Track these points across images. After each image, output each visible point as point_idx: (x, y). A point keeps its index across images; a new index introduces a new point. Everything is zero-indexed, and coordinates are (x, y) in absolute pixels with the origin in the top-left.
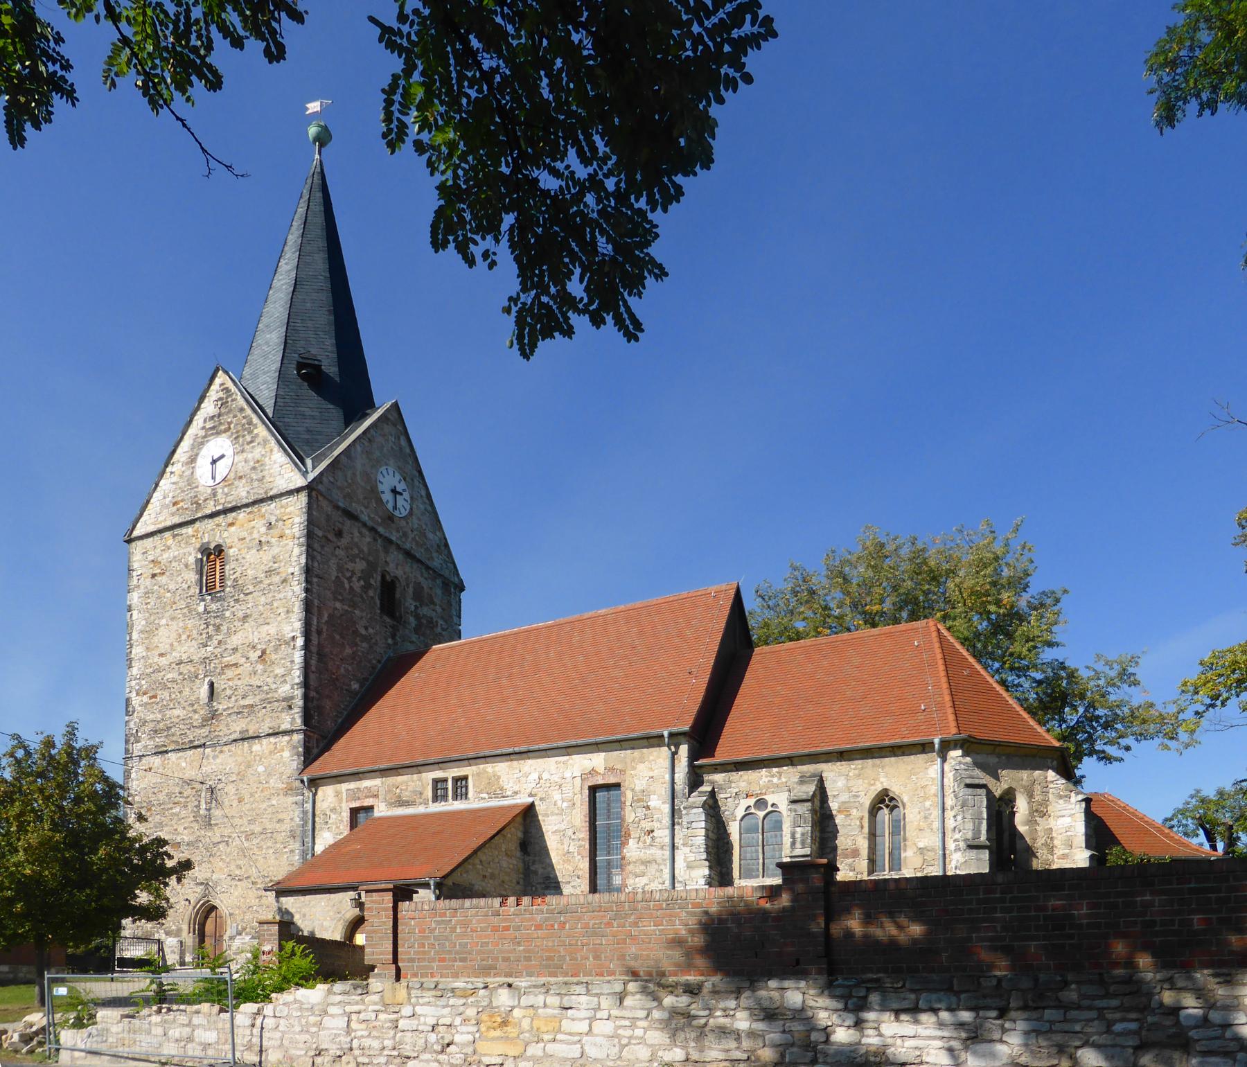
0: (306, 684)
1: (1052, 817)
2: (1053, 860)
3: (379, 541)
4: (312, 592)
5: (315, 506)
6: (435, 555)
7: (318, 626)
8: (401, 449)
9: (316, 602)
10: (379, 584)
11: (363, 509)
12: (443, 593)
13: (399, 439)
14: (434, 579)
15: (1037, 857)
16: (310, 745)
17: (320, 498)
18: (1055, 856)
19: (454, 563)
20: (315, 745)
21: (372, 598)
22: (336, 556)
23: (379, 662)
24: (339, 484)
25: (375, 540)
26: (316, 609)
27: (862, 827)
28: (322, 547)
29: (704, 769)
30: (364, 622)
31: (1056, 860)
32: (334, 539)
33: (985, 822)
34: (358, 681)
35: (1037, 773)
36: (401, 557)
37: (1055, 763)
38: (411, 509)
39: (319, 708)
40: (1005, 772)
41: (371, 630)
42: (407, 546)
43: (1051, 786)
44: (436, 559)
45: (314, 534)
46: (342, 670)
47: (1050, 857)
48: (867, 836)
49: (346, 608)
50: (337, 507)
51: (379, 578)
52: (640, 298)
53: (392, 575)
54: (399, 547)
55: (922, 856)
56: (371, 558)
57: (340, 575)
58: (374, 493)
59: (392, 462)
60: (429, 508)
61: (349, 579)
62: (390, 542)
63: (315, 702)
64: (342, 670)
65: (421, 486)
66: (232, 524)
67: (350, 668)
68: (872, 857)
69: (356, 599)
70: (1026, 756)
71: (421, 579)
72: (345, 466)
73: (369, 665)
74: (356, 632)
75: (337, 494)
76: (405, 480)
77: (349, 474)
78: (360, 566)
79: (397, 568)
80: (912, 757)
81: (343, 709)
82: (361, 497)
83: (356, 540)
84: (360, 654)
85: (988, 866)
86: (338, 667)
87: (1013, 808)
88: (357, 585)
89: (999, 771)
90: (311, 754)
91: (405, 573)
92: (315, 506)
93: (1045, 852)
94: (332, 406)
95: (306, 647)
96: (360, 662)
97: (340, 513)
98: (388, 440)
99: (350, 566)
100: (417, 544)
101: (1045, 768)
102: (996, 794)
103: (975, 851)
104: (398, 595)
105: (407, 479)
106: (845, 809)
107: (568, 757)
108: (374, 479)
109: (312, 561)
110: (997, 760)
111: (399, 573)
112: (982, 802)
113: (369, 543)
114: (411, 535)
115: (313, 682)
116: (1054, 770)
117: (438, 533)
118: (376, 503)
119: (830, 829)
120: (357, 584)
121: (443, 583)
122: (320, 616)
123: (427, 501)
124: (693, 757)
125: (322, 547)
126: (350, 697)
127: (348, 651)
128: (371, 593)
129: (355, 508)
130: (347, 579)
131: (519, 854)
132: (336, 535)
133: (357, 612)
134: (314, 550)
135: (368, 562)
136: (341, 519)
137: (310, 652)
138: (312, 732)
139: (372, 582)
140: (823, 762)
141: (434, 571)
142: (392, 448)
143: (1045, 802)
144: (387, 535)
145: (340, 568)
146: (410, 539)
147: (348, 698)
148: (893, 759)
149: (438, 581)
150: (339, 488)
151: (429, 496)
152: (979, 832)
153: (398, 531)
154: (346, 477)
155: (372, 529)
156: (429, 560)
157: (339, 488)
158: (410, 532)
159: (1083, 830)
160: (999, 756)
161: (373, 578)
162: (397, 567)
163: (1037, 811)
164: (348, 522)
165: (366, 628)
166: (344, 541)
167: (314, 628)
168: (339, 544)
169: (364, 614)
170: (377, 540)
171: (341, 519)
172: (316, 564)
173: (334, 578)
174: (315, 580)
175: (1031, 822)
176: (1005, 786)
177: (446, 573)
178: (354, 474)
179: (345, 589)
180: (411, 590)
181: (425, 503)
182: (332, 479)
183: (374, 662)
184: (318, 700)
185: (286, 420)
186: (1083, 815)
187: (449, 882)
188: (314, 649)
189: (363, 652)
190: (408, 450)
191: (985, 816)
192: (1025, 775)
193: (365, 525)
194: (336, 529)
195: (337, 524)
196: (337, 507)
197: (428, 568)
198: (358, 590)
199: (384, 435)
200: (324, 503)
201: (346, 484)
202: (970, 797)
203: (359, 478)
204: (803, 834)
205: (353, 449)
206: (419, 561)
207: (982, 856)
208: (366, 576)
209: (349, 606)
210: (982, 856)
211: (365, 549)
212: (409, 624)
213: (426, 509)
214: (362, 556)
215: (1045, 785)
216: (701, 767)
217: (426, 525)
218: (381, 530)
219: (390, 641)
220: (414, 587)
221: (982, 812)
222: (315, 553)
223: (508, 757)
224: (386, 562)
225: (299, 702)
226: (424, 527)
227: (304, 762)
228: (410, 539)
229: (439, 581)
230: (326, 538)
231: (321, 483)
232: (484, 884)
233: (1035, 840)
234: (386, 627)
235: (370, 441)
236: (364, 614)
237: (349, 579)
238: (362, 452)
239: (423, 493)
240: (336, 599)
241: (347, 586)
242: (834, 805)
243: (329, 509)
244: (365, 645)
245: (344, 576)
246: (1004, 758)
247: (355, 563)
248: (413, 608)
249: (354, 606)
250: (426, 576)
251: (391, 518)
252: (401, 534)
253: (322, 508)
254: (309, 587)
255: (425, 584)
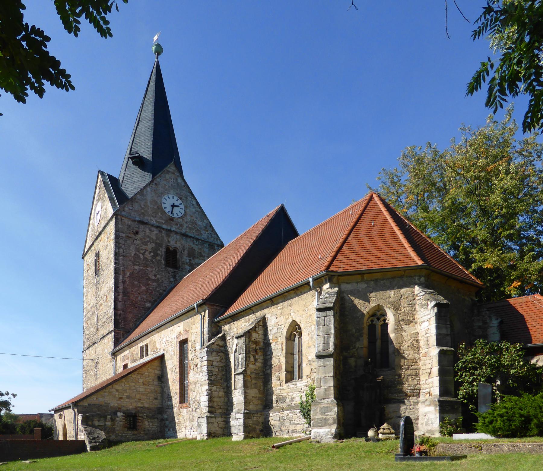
0: (116, 309)
1: (418, 324)
2: (419, 358)
3: (163, 232)
4: (119, 264)
5: (120, 223)
6: (203, 232)
7: (123, 279)
8: (178, 184)
9: (121, 268)
10: (163, 253)
11: (152, 218)
12: (209, 250)
13: (177, 179)
14: (203, 244)
15: (405, 359)
16: (119, 337)
17: (123, 218)
18: (421, 355)
19: (216, 234)
20: (122, 336)
21: (159, 260)
22: (135, 244)
23: (164, 291)
24: (136, 209)
25: (161, 232)
26: (122, 271)
27: (282, 349)
28: (125, 241)
29: (222, 323)
30: (154, 272)
31: (422, 358)
32: (133, 236)
33: (332, 336)
34: (150, 302)
35: (403, 291)
36: (178, 237)
37: (423, 279)
38: (186, 212)
39: (125, 319)
40: (372, 295)
41: (158, 276)
42: (183, 231)
43: (417, 298)
44: (204, 234)
45: (119, 236)
46: (139, 298)
47: (416, 355)
48: (285, 355)
49: (141, 268)
50: (134, 221)
51: (164, 250)
52: (76, 35)
53: (173, 247)
54: (176, 233)
55: (310, 366)
56: (158, 241)
57: (137, 253)
58: (160, 209)
59: (172, 192)
60: (199, 210)
61: (143, 254)
62: (170, 231)
63: (121, 316)
64: (139, 298)
65: (193, 200)
66: (101, 241)
67: (145, 297)
68: (290, 369)
69: (148, 263)
70: (393, 278)
71: (193, 246)
72: (139, 200)
73: (157, 293)
74: (148, 279)
75: (134, 214)
76: (181, 199)
77: (143, 203)
78: (150, 246)
79: (176, 243)
80: (305, 294)
81: (141, 317)
82: (151, 212)
83: (147, 234)
84: (151, 288)
85: (333, 371)
86: (137, 297)
87: (385, 320)
88: (149, 256)
89: (368, 294)
90: (117, 341)
91: (181, 245)
92: (120, 223)
93: (412, 352)
94: (147, 173)
95: (116, 291)
96: (152, 293)
97: (136, 223)
98: (169, 182)
99: (144, 247)
100: (190, 229)
101: (410, 284)
102: (364, 312)
103: (322, 360)
104: (178, 256)
105: (183, 198)
106: (275, 339)
107: (172, 327)
108: (159, 203)
109: (119, 249)
110: (366, 285)
111: (178, 245)
112: (330, 321)
113: (157, 234)
114: (185, 226)
115: (120, 305)
116: (421, 285)
117: (205, 221)
118: (161, 214)
119: (269, 353)
120: (149, 255)
121: (209, 245)
122: (124, 274)
123: (197, 206)
124: (211, 317)
125: (125, 241)
126: (145, 310)
127: (143, 288)
128: (158, 258)
129: (146, 219)
130: (142, 254)
131: (156, 383)
132: (134, 234)
133: (149, 269)
134: (119, 243)
135: (156, 244)
136: (137, 226)
137: (119, 292)
138: (119, 331)
139: (159, 252)
140: (266, 308)
141: (202, 240)
142: (172, 185)
143: (413, 312)
144: (169, 228)
145: (137, 250)
146: (185, 227)
147: (144, 311)
148: (296, 298)
149: (205, 245)
150: (135, 211)
151: (198, 204)
152: (328, 344)
153: (177, 225)
154: (140, 205)
155: (157, 227)
156: (198, 235)
157: (135, 211)
158: (185, 224)
159: (433, 330)
160: (367, 282)
161: (160, 250)
162: (175, 242)
163: (403, 320)
164: (142, 227)
165: (155, 276)
166: (139, 236)
167: (120, 281)
168: (136, 238)
169: (154, 269)
170: (162, 232)
171: (137, 226)
172: (121, 250)
173: (133, 255)
174: (121, 258)
175: (398, 329)
176: (373, 304)
177: (211, 240)
178: (146, 203)
179: (141, 259)
180: (186, 252)
181: (196, 208)
182: (131, 208)
183: (161, 291)
184: (124, 314)
185: (126, 186)
186: (435, 317)
187: (85, 403)
188: (121, 291)
189: (153, 288)
190: (183, 184)
191: (332, 331)
192: (392, 293)
193: (152, 226)
194: (134, 231)
195: (135, 229)
196: (134, 221)
197: (197, 240)
198: (150, 258)
199: (166, 180)
200: (126, 220)
201: (140, 208)
202: (321, 319)
203: (149, 204)
204: (242, 359)
205: (145, 191)
206: (191, 237)
207: (328, 363)
208: (155, 251)
209: (144, 267)
210: (328, 363)
211: (154, 238)
212: (185, 269)
213: (196, 211)
214: (151, 241)
215: (412, 298)
216: (219, 322)
217: (197, 218)
218: (164, 226)
219: (172, 280)
220: (188, 251)
221: (330, 329)
222: (121, 245)
223: (158, 330)
224: (168, 241)
225: (113, 317)
226: (195, 219)
227: (115, 345)
228: (185, 227)
229: (206, 245)
230: (128, 236)
231: (124, 211)
232: (119, 402)
233: (401, 344)
234: (169, 273)
235: (156, 184)
236: (154, 269)
237: (143, 254)
238: (151, 191)
239: (194, 203)
240: (134, 265)
241: (142, 257)
242: (270, 337)
243: (130, 223)
244: (155, 284)
245: (140, 253)
246: (372, 282)
247: (147, 245)
248: (188, 261)
249: (146, 266)
250: (197, 243)
251: (172, 219)
252: (179, 225)
253: (125, 223)
254: (117, 261)
255: (196, 248)
